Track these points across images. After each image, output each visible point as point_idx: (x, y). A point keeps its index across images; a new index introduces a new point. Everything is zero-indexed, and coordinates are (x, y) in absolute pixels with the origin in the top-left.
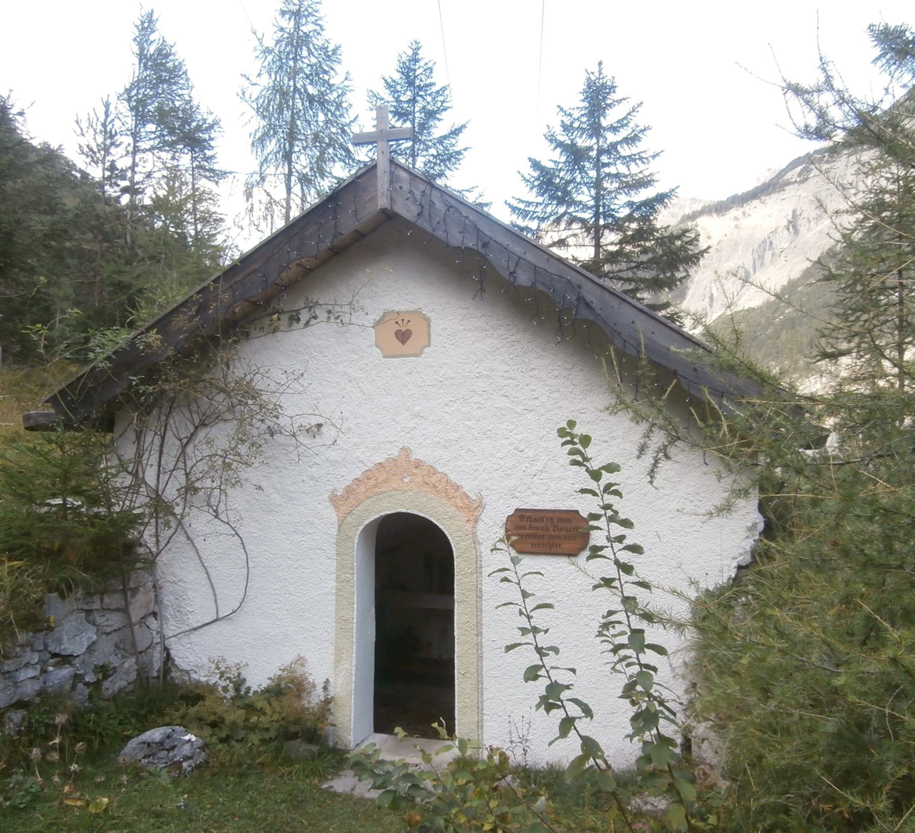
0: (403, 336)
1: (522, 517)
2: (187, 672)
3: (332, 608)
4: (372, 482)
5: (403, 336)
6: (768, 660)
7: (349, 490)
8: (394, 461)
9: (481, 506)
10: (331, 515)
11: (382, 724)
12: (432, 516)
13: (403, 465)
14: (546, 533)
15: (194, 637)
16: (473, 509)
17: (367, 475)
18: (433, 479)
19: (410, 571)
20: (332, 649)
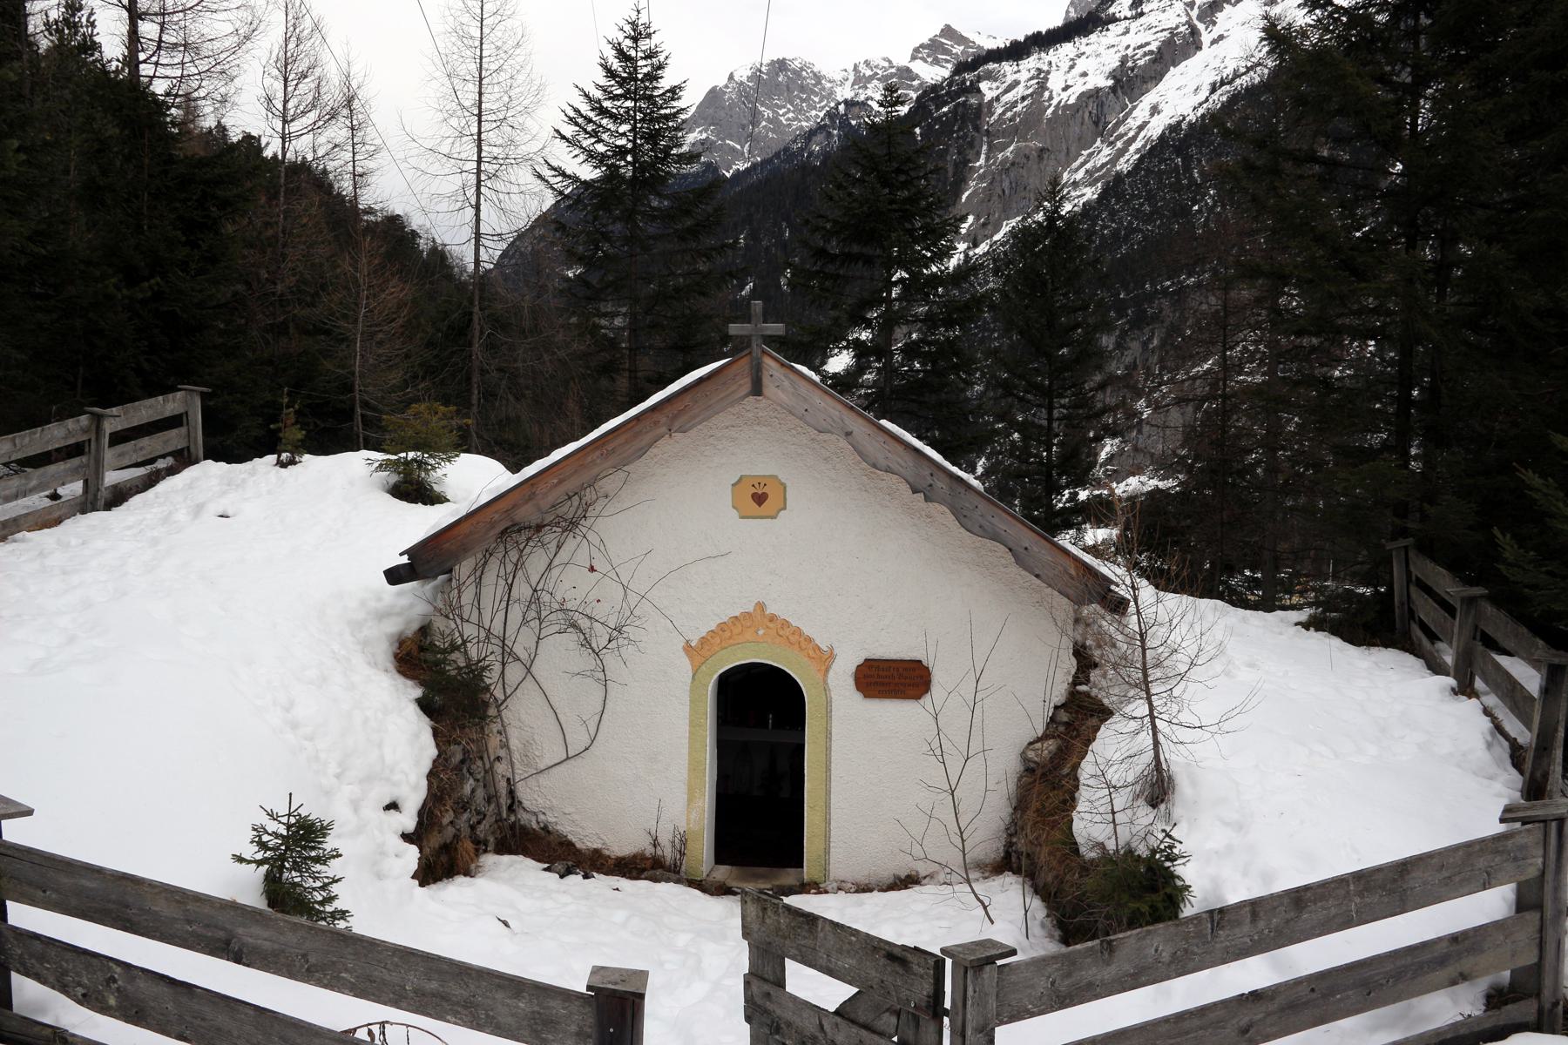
0: (760, 499)
1: (870, 667)
2: (535, 814)
3: (685, 751)
4: (727, 634)
5: (760, 499)
6: (1441, 645)
7: (703, 641)
8: (747, 615)
9: (831, 656)
10: (685, 665)
11: (720, 858)
12: (190, 486)
13: (759, 618)
14: (895, 679)
15: (543, 779)
16: (825, 659)
17: (722, 627)
18: (787, 632)
19: (759, 717)
20: (684, 788)
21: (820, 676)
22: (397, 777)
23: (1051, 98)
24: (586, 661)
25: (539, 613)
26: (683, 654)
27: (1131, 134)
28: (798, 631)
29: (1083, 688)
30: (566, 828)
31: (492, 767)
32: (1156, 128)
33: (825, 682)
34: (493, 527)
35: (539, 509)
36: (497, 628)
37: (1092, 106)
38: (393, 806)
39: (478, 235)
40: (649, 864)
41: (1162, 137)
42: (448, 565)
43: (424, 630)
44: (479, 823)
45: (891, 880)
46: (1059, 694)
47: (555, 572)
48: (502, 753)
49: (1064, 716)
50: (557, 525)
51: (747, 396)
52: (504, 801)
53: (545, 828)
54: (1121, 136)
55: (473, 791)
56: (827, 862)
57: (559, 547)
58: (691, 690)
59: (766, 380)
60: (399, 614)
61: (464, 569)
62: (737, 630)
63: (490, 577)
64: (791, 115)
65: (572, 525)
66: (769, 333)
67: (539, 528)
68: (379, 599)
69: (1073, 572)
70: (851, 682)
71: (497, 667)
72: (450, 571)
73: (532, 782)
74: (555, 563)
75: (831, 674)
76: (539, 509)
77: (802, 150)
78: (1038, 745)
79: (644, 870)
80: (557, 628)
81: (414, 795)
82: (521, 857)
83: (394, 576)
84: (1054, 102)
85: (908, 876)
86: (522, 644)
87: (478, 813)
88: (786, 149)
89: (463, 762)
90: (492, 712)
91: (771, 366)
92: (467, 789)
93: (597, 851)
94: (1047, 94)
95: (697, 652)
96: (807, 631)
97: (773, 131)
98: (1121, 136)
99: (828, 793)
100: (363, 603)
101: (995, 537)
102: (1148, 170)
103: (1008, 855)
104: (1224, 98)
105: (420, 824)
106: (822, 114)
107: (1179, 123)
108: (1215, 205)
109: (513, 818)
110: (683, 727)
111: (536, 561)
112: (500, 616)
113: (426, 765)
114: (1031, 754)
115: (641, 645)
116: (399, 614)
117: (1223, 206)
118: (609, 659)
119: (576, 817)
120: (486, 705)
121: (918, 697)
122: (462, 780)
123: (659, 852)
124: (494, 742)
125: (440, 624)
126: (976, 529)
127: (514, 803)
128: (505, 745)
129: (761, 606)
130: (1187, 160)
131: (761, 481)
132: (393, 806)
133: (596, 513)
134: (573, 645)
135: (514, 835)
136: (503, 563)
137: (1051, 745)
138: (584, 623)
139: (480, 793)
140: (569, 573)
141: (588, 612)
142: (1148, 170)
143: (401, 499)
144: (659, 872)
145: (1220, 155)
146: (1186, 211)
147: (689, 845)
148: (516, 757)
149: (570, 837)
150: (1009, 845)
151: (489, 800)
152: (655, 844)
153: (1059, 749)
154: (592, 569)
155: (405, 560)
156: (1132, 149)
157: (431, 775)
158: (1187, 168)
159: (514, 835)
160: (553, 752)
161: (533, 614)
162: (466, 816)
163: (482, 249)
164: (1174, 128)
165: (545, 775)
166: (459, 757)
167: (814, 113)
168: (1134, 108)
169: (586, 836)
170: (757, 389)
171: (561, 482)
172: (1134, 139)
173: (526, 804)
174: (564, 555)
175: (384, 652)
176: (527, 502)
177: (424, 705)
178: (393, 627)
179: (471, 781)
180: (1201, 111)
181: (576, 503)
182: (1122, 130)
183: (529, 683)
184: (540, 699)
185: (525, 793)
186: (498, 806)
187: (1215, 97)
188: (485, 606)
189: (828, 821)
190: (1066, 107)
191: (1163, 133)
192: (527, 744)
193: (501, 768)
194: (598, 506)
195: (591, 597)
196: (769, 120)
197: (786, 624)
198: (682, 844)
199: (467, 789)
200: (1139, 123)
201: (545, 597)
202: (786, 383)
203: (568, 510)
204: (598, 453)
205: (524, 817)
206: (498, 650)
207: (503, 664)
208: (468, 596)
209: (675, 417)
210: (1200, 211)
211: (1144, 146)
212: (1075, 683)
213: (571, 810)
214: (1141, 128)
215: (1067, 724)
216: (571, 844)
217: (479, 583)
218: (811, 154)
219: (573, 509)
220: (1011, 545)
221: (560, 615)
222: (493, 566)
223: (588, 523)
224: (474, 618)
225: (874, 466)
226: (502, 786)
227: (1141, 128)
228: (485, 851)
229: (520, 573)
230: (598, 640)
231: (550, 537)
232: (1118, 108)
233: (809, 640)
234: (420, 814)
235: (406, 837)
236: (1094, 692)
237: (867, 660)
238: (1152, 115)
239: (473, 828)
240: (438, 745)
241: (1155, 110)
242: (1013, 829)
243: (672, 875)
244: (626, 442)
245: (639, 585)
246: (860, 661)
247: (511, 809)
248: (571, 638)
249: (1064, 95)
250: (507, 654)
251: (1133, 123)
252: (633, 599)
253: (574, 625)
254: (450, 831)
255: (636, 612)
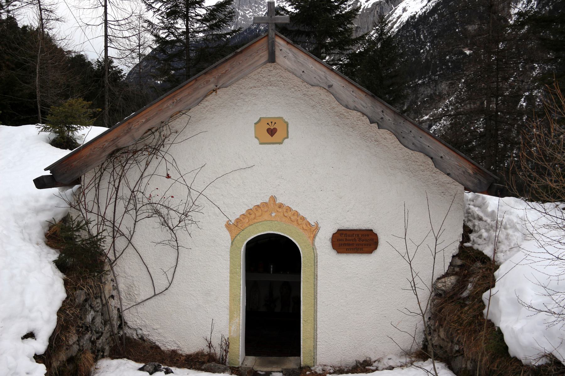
0: (272, 132)
1: (341, 234)
2: (135, 330)
3: (227, 289)
4: (253, 216)
5: (272, 132)
7: (238, 220)
8: (265, 204)
10: (226, 236)
11: (248, 352)
13: (272, 206)
14: (356, 241)
15: (140, 309)
16: (313, 230)
17: (249, 212)
18: (290, 214)
20: (227, 312)
21: (310, 241)
22: (33, 315)
23: (361, 6)
24: (165, 234)
25: (135, 205)
26: (225, 229)
27: (394, 20)
28: (296, 213)
29: (467, 244)
30: (155, 338)
31: (107, 302)
32: (405, 18)
33: (313, 244)
34: (104, 151)
35: (133, 139)
36: (109, 215)
37: (378, 9)
38: (30, 335)
39: (106, 21)
40: (206, 358)
41: (408, 21)
42: (76, 176)
43: (66, 219)
44: (98, 338)
45: (354, 364)
46: (454, 249)
47: (145, 181)
48: (114, 293)
49: (459, 262)
50: (146, 150)
51: (265, 63)
52: (116, 323)
53: (142, 338)
54: (390, 21)
55: (93, 319)
56: (315, 354)
57: (147, 165)
58: (231, 252)
59: (277, 53)
60: (49, 210)
61: (88, 178)
62: (258, 214)
63: (104, 184)
64: (251, 14)
65: (155, 150)
66: (280, 21)
67: (135, 152)
68: (37, 201)
69: (470, 171)
70: (329, 244)
71: (109, 240)
72: (78, 181)
73: (133, 310)
74: (146, 174)
75: (317, 239)
76: (133, 139)
77: (256, 28)
78: (443, 280)
79: (203, 363)
80: (147, 214)
81: (46, 325)
82: (124, 361)
83: (40, 183)
84: (362, 7)
85: (365, 361)
86: (125, 226)
87: (97, 332)
88: (249, 28)
89: (86, 300)
90: (107, 268)
91: (281, 44)
92: (89, 318)
93: (174, 352)
94: (359, 4)
95: (234, 227)
96: (302, 213)
97: (244, 20)
98: (390, 21)
99: (315, 311)
100: (26, 203)
101: (422, 151)
102: (402, 36)
103: (425, 347)
104: (434, 4)
105: (50, 347)
106: (264, 13)
107: (415, 15)
108: (430, 50)
109: (121, 333)
110: (226, 274)
111: (133, 173)
112: (111, 207)
113: (57, 304)
114: (440, 285)
115: (199, 224)
116: (49, 210)
117: (434, 51)
118: (180, 233)
119: (161, 331)
120: (103, 263)
121: (370, 252)
122: (86, 312)
123: (212, 351)
124: (108, 288)
125: (74, 214)
126: (411, 146)
127: (122, 324)
128: (116, 288)
129: (273, 198)
130: (418, 31)
131: (273, 121)
132: (30, 335)
133: (170, 142)
134: (157, 225)
135: (122, 344)
136: (112, 174)
137: (451, 280)
138: (164, 211)
139: (99, 320)
140: (155, 181)
141: (166, 204)
142: (402, 36)
143: (57, 147)
144: (213, 364)
145: (432, 28)
146: (418, 53)
147: (230, 346)
148: (123, 295)
149: (157, 343)
150: (426, 340)
151: (105, 323)
152: (210, 346)
153: (458, 281)
154: (168, 177)
155: (48, 173)
156: (395, 26)
157: (61, 312)
158: (418, 35)
159: (122, 344)
160: (145, 291)
161: (131, 206)
162: (87, 336)
163: (109, 30)
164: (413, 17)
165: (141, 305)
166: (83, 298)
167: (261, 13)
168: (396, 9)
169: (167, 341)
170: (272, 59)
171: (147, 121)
172: (396, 22)
173: (130, 324)
174: (150, 170)
175: (37, 233)
176: (126, 134)
177: (60, 265)
178: (45, 217)
179: (92, 312)
180: (424, 10)
181: (157, 137)
182: (390, 18)
183: (130, 250)
184: (137, 259)
185: (128, 317)
186: (112, 326)
187: (430, 4)
188: (102, 202)
189: (315, 329)
190: (367, 9)
191: (408, 20)
192: (130, 287)
193: (113, 303)
194: (171, 138)
195: (168, 194)
196: (242, 16)
197: (289, 209)
198: (227, 345)
199: (89, 318)
200: (398, 15)
201: (140, 195)
202: (291, 55)
203: (152, 140)
204: (171, 102)
205: (128, 332)
206: (110, 229)
207: (114, 238)
208: (90, 196)
209: (220, 78)
210: (423, 52)
211: (400, 25)
212: (462, 243)
213: (158, 327)
214: (399, 18)
215: (461, 266)
216: (158, 348)
217: (98, 188)
218: (260, 30)
219: (155, 141)
220: (432, 155)
221: (149, 207)
222: (107, 177)
223: (165, 149)
224: (95, 210)
225: (347, 107)
226: (115, 314)
227: (399, 18)
228: (103, 357)
229: (123, 181)
230: (172, 221)
231: (143, 158)
232: (389, 9)
233: (303, 219)
234: (51, 339)
235: (38, 358)
236: (476, 247)
237: (339, 230)
238: (403, 12)
239: (93, 342)
240: (67, 291)
241: (404, 10)
242: (429, 331)
243: (222, 367)
244: (189, 94)
245: (198, 186)
246: (335, 231)
247: (120, 327)
248: (156, 220)
249: (366, 4)
250: (116, 232)
251: (395, 16)
252: (194, 194)
253: (157, 212)
254: (76, 348)
255: (196, 203)
